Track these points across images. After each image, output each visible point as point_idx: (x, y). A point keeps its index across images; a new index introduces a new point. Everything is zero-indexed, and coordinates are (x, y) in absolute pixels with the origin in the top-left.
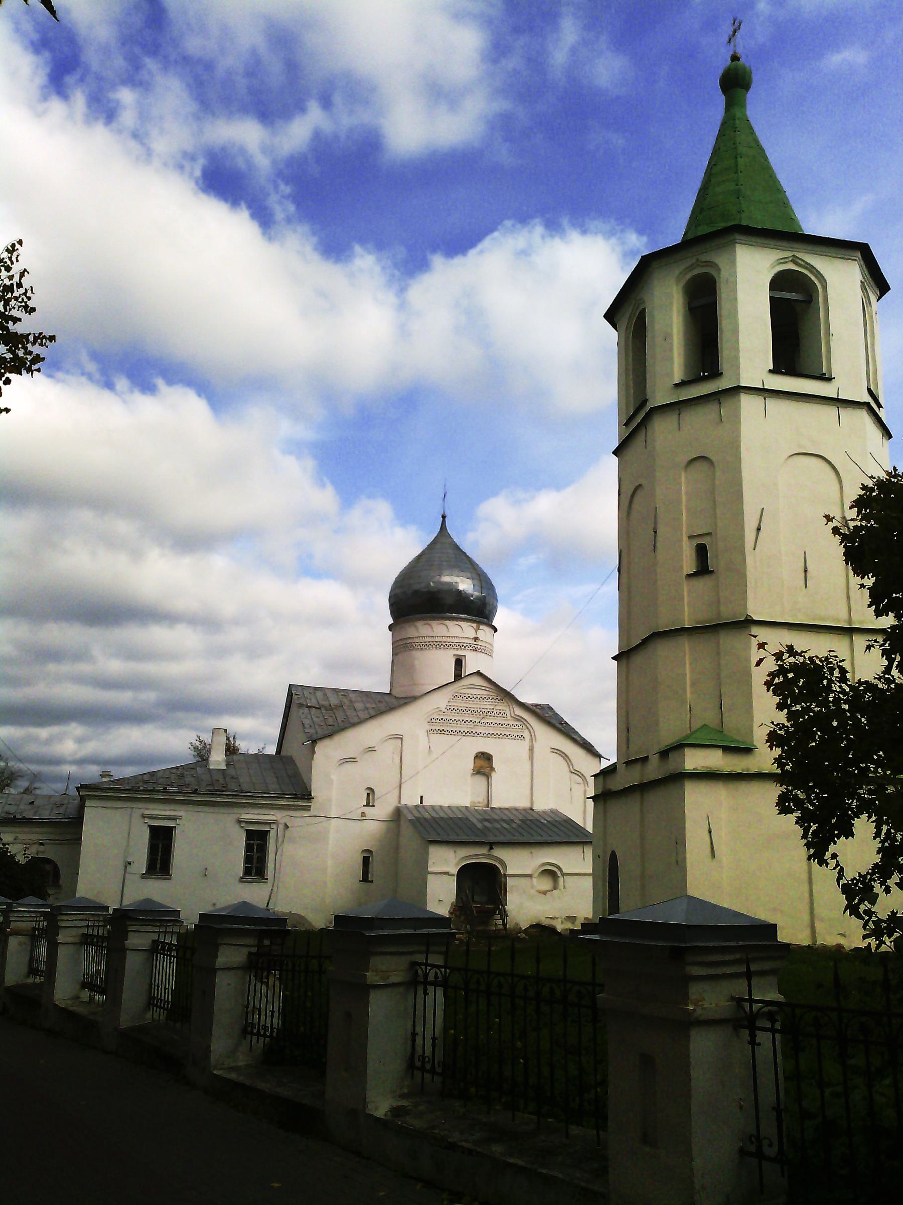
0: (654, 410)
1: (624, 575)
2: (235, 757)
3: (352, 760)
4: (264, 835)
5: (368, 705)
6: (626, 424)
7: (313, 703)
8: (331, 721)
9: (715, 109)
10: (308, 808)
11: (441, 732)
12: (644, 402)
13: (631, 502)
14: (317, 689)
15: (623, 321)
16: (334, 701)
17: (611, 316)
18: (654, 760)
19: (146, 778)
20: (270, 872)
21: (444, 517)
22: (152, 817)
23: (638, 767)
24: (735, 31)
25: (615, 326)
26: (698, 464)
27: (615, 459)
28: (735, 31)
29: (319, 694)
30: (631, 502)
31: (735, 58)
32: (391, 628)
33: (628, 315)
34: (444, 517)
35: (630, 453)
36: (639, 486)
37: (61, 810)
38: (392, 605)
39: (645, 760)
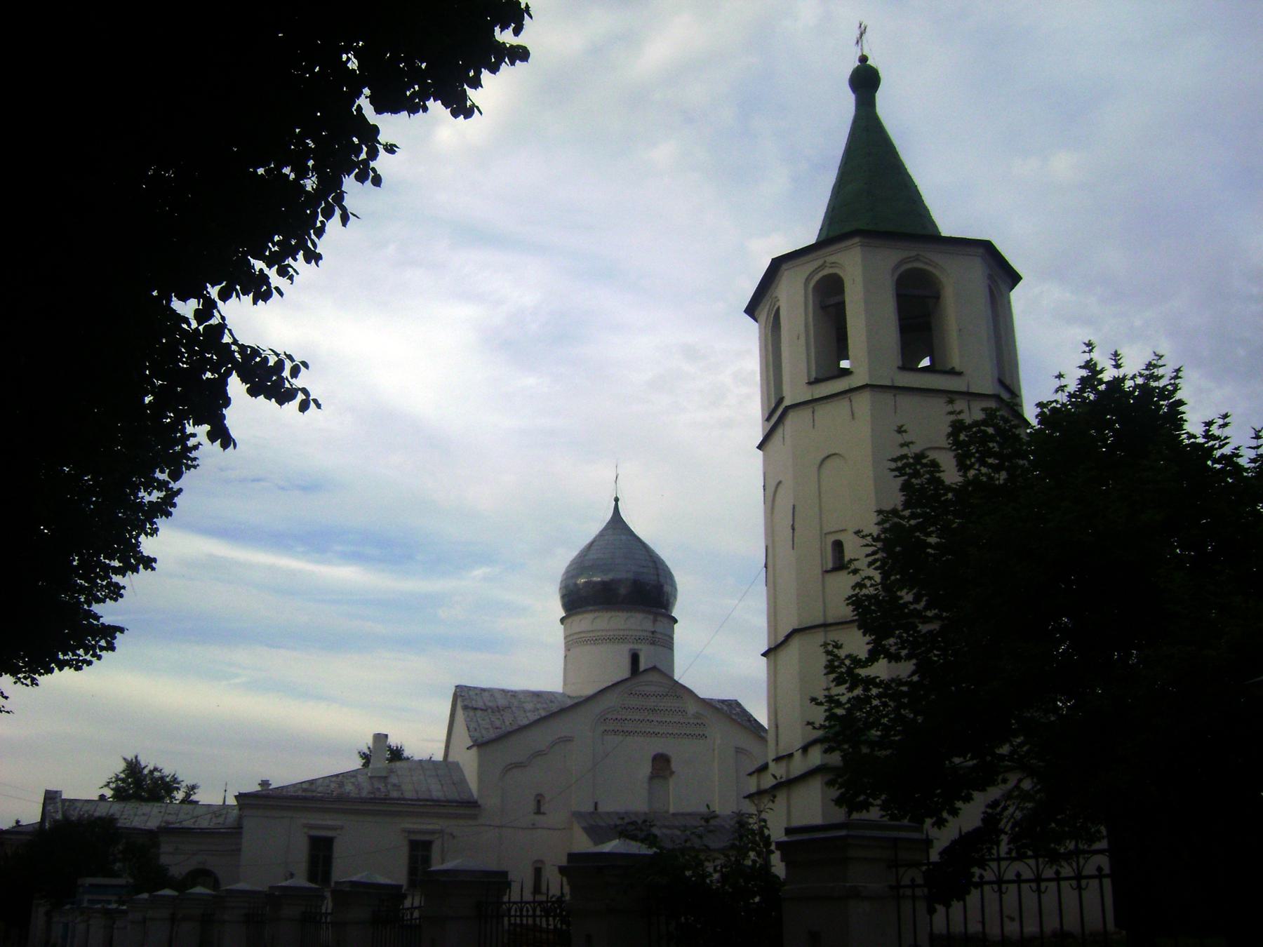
0: (787, 409)
1: (770, 569)
2: (398, 764)
3: (518, 765)
4: (427, 845)
5: (539, 706)
6: (768, 419)
7: (480, 705)
8: (498, 723)
9: (847, 103)
10: (474, 817)
11: (615, 732)
12: (780, 400)
13: (774, 500)
14: (483, 690)
15: (763, 313)
16: (502, 702)
17: (751, 310)
18: (798, 755)
19: (304, 786)
20: (427, 838)
21: (617, 500)
22: (311, 827)
23: (783, 764)
24: (861, 35)
25: (756, 320)
26: (828, 463)
27: (760, 453)
28: (861, 35)
29: (486, 694)
30: (774, 500)
31: (863, 59)
32: (562, 620)
33: (766, 310)
34: (617, 500)
35: (770, 446)
36: (780, 482)
37: (221, 820)
38: (563, 597)
39: (791, 755)
